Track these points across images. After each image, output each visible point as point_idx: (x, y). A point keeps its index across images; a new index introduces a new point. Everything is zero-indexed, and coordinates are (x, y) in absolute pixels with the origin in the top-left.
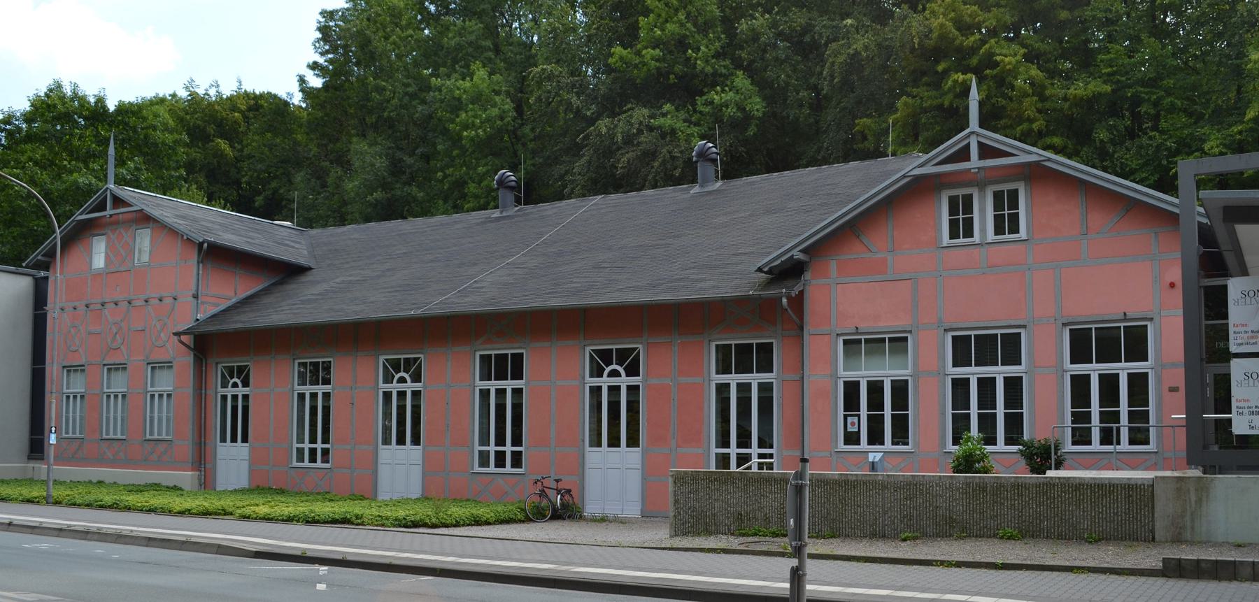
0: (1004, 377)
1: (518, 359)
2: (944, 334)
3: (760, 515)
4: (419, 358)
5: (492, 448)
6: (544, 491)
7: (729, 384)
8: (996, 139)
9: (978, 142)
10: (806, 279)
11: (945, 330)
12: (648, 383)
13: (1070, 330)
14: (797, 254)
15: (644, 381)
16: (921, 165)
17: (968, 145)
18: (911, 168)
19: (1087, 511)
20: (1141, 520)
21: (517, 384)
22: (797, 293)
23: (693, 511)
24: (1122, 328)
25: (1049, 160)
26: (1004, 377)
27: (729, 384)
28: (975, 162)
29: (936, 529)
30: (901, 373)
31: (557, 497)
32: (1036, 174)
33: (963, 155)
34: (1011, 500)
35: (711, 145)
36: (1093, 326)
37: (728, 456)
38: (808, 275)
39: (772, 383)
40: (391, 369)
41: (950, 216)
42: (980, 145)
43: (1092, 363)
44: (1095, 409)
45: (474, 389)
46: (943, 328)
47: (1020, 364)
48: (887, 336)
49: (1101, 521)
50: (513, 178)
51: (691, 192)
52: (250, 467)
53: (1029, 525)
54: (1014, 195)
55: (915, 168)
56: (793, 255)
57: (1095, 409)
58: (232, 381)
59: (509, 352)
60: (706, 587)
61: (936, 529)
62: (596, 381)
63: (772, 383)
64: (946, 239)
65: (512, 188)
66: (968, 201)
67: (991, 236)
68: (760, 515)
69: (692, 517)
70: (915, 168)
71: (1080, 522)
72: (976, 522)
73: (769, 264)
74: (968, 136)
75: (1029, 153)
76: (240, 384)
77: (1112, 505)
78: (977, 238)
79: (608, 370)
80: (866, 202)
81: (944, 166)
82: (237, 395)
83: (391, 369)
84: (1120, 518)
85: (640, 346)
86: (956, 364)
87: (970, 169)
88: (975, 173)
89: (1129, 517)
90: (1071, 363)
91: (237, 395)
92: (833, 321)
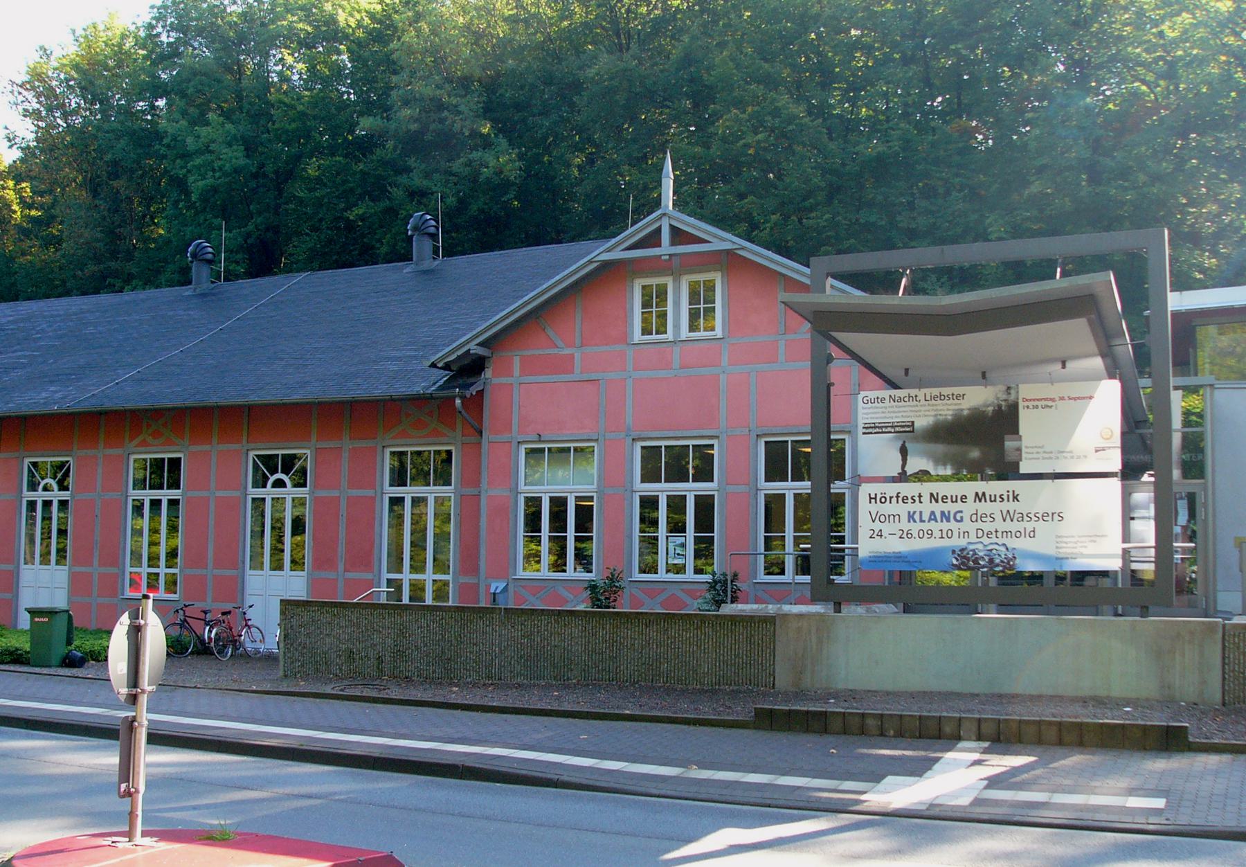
0: (695, 496)
1: (175, 464)
2: (633, 445)
3: (371, 653)
4: (67, 462)
5: (145, 570)
6: (185, 620)
7: (784, 495)
8: (690, 224)
9: (670, 225)
10: (487, 377)
11: (633, 439)
12: (315, 495)
13: (766, 442)
14: (474, 348)
15: (311, 493)
16: (609, 250)
17: (659, 229)
18: (597, 252)
19: (708, 653)
20: (762, 663)
21: (174, 494)
22: (474, 393)
23: (304, 648)
24: (691, 447)
25: (743, 248)
26: (695, 496)
27: (784, 495)
28: (666, 248)
29: (554, 671)
30: (588, 487)
31: (205, 629)
32: (730, 262)
33: (653, 239)
34: (631, 638)
35: (429, 217)
36: (789, 439)
37: (399, 582)
38: (488, 373)
39: (713, 496)
40: (260, 465)
41: (642, 308)
42: (672, 228)
43: (787, 481)
44: (571, 533)
45: (246, 497)
46: (631, 438)
47: (712, 481)
48: (572, 445)
49: (722, 664)
50: (210, 250)
51: (405, 271)
52: (69, 598)
53: (649, 668)
54: (710, 288)
55: (602, 252)
56: (469, 350)
57: (571, 533)
58: (272, 479)
59: (166, 456)
60: (29, 714)
61: (554, 671)
62: (259, 492)
63: (713, 496)
64: (637, 336)
65: (210, 262)
66: (662, 293)
67: (685, 333)
68: (371, 653)
69: (302, 655)
70: (602, 252)
71: (701, 665)
72: (595, 664)
73: (444, 359)
74: (660, 218)
75: (723, 240)
76: (55, 486)
77: (733, 646)
78: (670, 335)
79: (272, 479)
80: (549, 290)
81: (633, 251)
82: (160, 500)
83: (260, 465)
84: (741, 660)
85: (308, 452)
86: (644, 479)
87: (661, 255)
88: (665, 260)
89: (750, 660)
90: (765, 481)
91: (160, 500)
92: (515, 427)
